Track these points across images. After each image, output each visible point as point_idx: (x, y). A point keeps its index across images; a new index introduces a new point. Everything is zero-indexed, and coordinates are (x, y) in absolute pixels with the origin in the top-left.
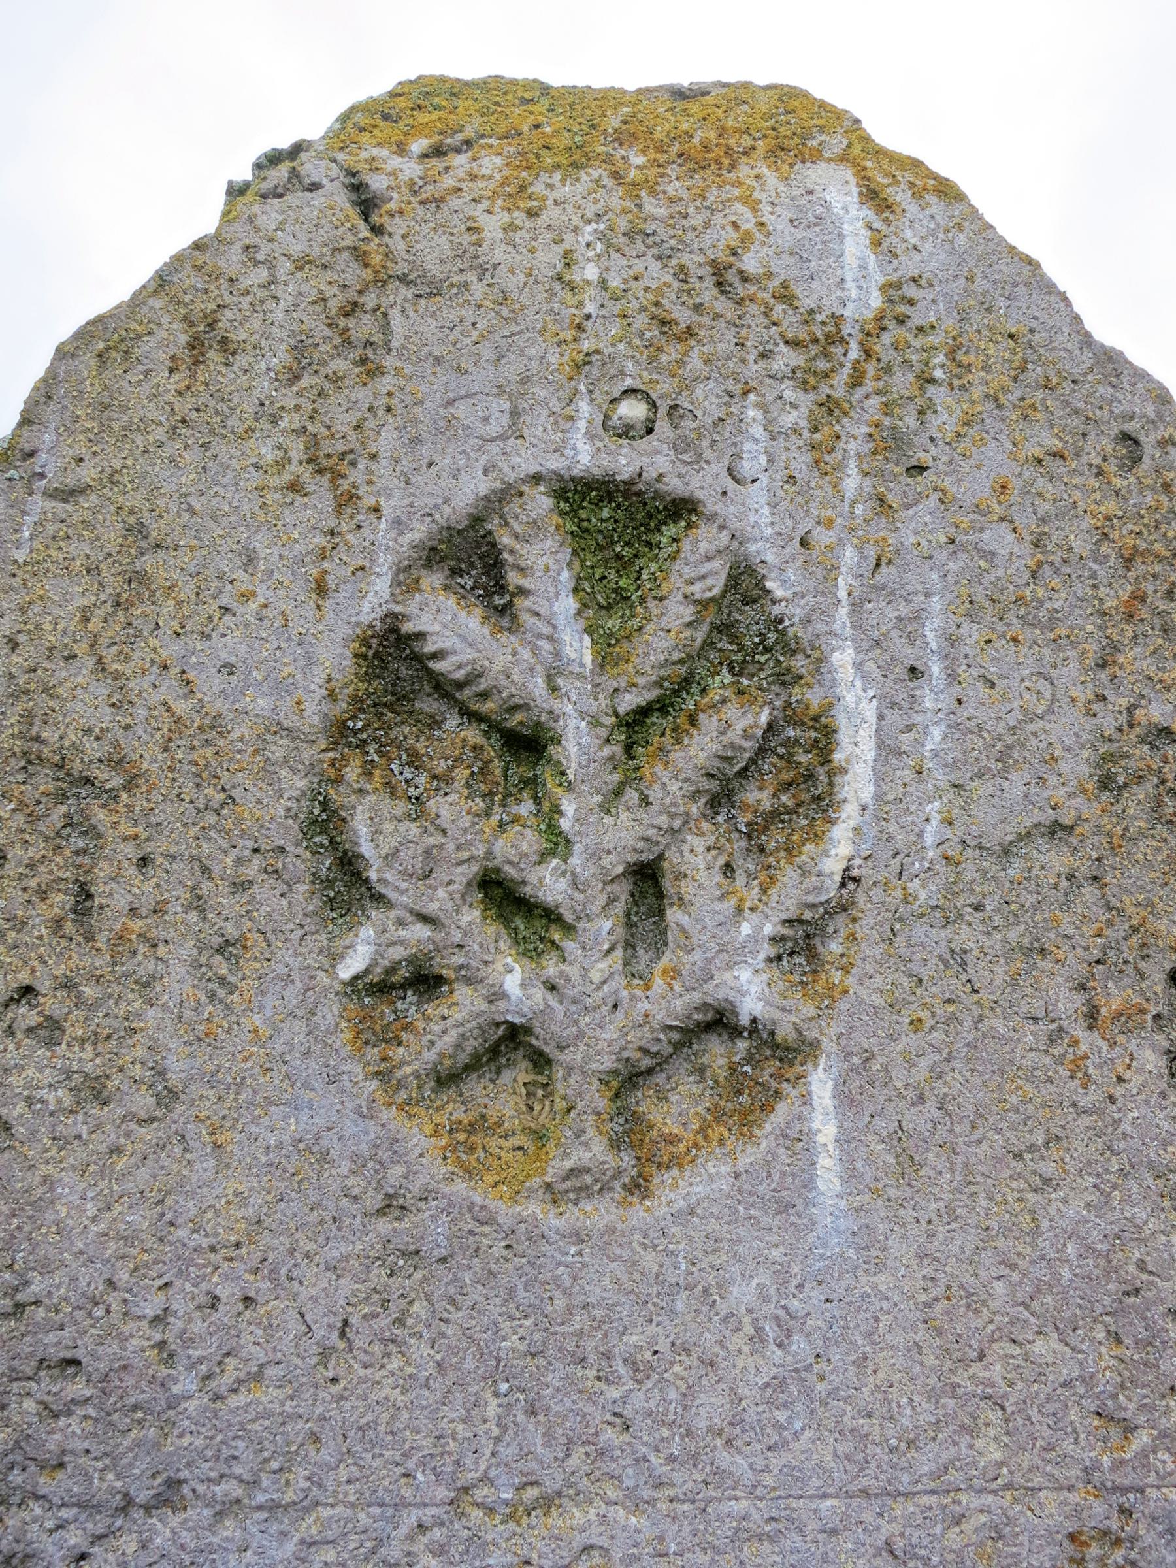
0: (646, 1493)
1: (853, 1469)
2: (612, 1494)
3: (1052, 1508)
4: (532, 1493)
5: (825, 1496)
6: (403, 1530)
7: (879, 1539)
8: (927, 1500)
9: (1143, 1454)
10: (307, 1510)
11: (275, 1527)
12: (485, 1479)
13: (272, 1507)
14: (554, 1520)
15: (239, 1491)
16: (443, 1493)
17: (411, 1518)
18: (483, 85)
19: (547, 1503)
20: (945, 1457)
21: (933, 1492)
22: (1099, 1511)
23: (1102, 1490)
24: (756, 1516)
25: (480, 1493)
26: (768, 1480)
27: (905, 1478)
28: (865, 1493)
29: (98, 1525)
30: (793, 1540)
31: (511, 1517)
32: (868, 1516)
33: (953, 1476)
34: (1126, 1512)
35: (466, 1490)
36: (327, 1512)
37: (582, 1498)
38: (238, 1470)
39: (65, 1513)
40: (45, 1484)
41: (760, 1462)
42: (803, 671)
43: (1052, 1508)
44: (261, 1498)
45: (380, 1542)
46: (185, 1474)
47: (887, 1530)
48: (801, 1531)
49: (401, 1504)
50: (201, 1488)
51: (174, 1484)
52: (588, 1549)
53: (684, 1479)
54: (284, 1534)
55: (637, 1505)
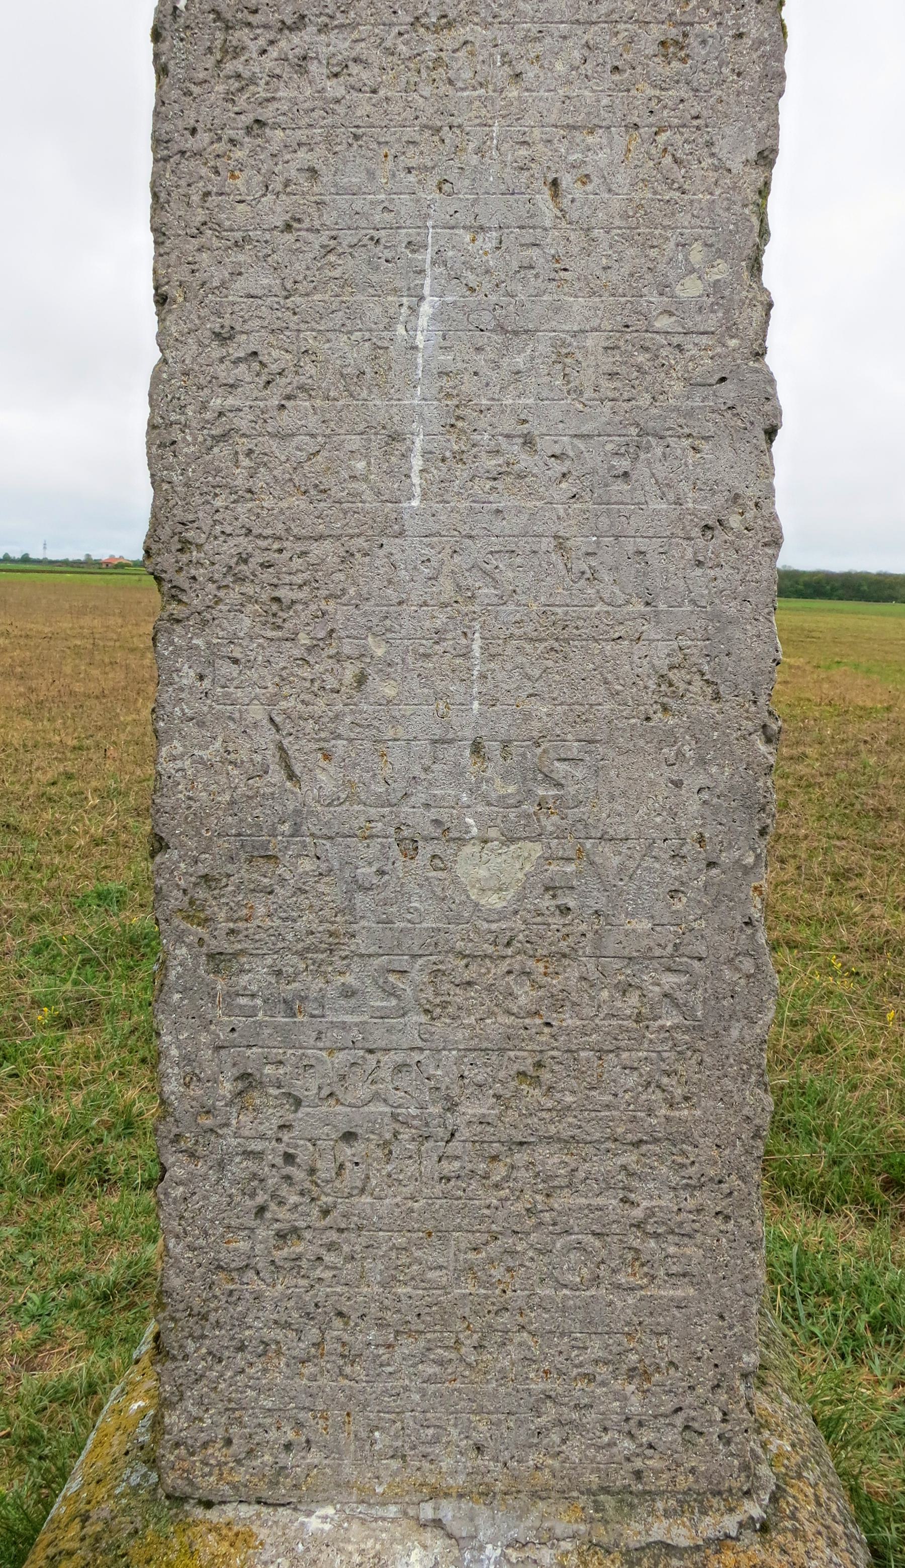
0: (490, 20)
1: (574, 11)
2: (476, 20)
3: (655, 30)
4: (444, 21)
5: (562, 22)
6: (393, 35)
7: (583, 42)
8: (603, 25)
9: (694, 9)
10: (354, 28)
11: (341, 36)
12: (426, 14)
13: (341, 26)
14: (453, 33)
15: (327, 20)
16: (410, 19)
17: (396, 30)
18: (153, 403)
19: (450, 25)
20: (611, 7)
21: (606, 22)
22: (673, 32)
23: (676, 24)
24: (533, 29)
25: (423, 21)
26: (539, 15)
27: (595, 15)
28: (578, 21)
29: (271, 35)
30: (548, 40)
31: (436, 32)
32: (579, 32)
33: (615, 17)
34: (685, 35)
35: (417, 18)
36: (361, 28)
37: (464, 23)
38: (327, 11)
39: (258, 31)
40: (251, 18)
41: (536, 7)
42: (813, 1349)
43: (655, 30)
44: (336, 23)
45: (383, 40)
46: (306, 12)
47: (586, 37)
48: (552, 36)
49: (391, 25)
50: (312, 18)
51: (303, 17)
52: (466, 43)
53: (505, 14)
54: (345, 39)
55: (487, 25)
